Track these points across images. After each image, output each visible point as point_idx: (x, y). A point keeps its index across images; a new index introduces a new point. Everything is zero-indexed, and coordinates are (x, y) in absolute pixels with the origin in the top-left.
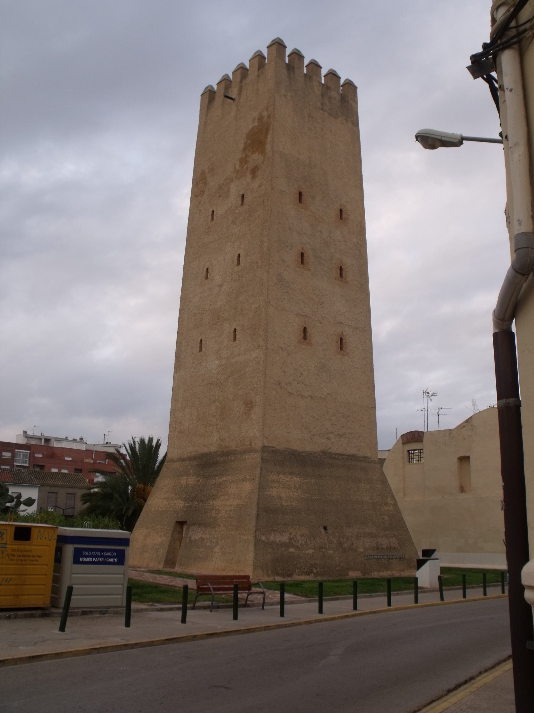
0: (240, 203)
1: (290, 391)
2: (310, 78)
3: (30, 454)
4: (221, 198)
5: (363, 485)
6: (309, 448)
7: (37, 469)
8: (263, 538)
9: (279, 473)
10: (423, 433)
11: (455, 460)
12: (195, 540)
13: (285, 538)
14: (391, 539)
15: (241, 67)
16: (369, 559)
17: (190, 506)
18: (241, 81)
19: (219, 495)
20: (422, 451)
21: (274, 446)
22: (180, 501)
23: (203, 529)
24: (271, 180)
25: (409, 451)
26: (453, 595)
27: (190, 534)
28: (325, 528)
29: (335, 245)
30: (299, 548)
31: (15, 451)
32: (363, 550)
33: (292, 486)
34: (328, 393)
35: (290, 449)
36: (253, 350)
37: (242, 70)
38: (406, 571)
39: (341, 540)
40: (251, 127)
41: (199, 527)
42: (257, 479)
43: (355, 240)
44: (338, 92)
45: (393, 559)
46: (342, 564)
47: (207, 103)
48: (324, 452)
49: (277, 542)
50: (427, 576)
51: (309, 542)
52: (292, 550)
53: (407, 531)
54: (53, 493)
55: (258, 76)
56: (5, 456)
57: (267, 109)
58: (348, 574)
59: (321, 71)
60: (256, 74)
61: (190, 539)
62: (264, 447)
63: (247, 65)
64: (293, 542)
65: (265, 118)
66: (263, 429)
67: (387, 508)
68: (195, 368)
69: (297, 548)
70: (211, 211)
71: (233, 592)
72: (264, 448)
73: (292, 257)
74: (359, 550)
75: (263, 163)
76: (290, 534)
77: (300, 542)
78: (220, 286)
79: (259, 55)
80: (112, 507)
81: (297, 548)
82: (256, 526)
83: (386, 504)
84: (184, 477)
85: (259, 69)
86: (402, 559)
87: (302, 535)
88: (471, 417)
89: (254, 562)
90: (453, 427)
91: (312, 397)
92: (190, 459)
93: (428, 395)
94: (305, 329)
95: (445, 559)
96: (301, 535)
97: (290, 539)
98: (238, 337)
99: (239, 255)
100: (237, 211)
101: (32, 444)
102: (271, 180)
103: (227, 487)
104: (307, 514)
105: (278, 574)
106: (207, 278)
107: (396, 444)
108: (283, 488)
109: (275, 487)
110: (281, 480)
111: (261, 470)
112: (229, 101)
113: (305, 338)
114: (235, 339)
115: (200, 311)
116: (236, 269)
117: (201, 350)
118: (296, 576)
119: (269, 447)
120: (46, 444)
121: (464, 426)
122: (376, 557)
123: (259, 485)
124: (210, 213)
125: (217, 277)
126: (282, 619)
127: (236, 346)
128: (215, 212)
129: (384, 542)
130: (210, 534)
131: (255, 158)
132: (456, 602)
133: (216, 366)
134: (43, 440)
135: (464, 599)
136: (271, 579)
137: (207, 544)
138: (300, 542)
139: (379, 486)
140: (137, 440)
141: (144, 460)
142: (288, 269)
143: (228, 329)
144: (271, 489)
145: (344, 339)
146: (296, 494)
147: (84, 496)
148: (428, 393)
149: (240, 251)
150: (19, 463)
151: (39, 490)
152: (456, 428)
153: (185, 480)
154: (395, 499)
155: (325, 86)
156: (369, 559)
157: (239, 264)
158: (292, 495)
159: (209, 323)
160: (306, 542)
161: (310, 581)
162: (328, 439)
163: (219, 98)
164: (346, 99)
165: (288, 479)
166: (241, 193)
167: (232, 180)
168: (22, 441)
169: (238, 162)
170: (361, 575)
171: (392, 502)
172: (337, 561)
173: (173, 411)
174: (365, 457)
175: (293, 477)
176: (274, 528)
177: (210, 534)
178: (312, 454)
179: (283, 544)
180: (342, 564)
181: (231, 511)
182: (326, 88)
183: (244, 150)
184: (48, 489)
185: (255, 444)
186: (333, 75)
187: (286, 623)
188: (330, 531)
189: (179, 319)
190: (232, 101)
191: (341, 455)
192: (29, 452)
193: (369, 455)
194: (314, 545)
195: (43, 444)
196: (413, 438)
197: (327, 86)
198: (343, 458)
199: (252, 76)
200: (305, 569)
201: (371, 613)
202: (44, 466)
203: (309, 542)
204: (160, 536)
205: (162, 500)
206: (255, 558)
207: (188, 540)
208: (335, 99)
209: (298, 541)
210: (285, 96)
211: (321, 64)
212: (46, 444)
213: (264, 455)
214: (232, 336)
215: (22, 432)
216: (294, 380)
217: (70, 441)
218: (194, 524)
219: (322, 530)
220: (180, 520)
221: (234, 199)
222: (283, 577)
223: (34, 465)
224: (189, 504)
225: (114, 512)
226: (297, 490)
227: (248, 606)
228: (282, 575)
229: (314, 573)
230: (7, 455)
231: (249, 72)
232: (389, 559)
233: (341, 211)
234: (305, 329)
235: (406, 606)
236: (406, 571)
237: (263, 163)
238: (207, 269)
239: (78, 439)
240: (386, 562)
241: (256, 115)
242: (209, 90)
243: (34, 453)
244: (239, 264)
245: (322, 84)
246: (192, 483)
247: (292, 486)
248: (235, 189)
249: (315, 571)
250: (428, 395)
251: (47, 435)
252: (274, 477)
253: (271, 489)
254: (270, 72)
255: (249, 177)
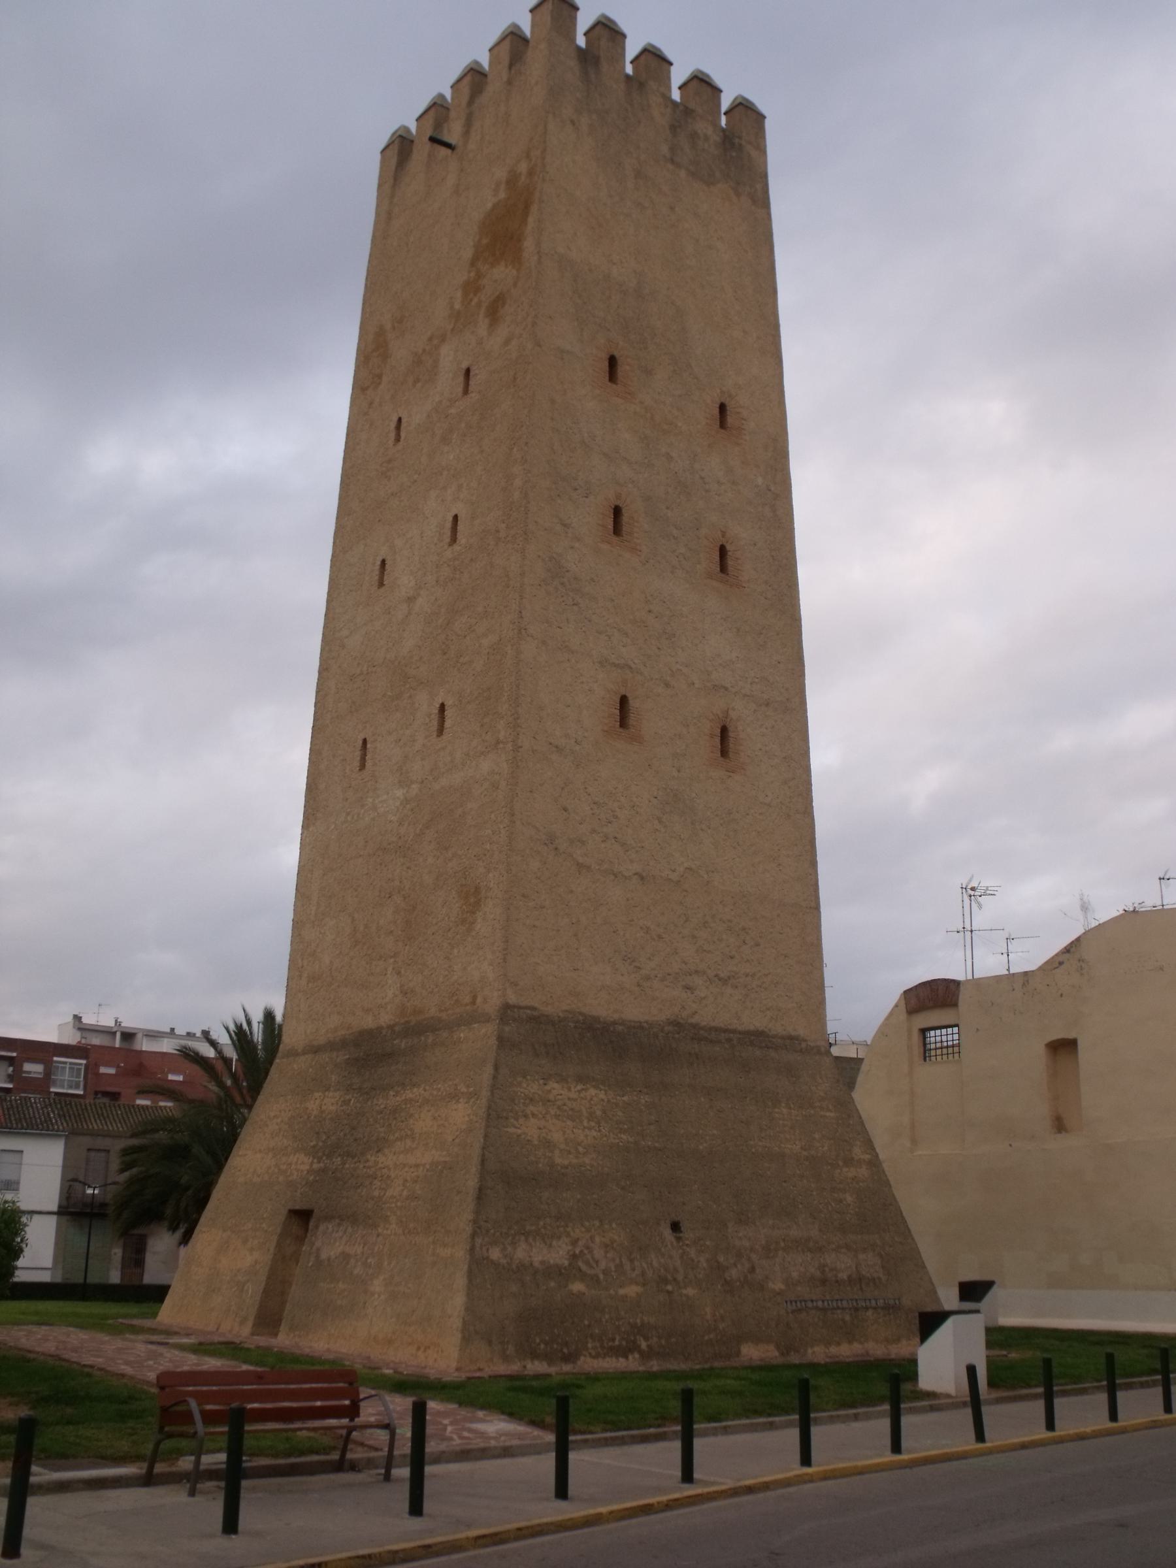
0: (460, 389)
1: (581, 860)
2: (642, 85)
3: (87, 1066)
4: (419, 385)
5: (785, 1111)
6: (634, 1012)
7: (106, 1100)
8: (495, 1254)
9: (546, 1079)
10: (957, 983)
11: (1040, 1049)
12: (329, 1260)
13: (558, 1254)
14: (861, 1256)
15: (472, 69)
16: (800, 1311)
17: (324, 1171)
18: (471, 102)
19: (391, 1137)
20: (956, 1030)
21: (536, 1005)
22: (302, 1157)
23: (350, 1230)
24: (534, 324)
25: (924, 1031)
26: (1015, 1421)
27: (318, 1244)
28: (675, 1227)
29: (707, 491)
30: (598, 1281)
31: (52, 1061)
32: (783, 1287)
33: (585, 1114)
34: (690, 869)
35: (581, 1013)
36: (482, 753)
37: (474, 77)
38: (904, 1342)
39: (721, 1259)
40: (489, 205)
41: (339, 1225)
42: (485, 1093)
43: (760, 481)
44: (715, 123)
45: (867, 1308)
46: (721, 1326)
47: (393, 168)
48: (677, 1024)
49: (536, 1264)
50: (943, 1361)
51: (627, 1266)
52: (577, 1287)
53: (906, 1233)
54: (99, 1150)
55: (509, 82)
56: (29, 1072)
57: (528, 156)
58: (738, 1354)
59: (669, 72)
60: (505, 78)
61: (318, 1257)
62: (507, 1007)
63: (485, 63)
64: (580, 1264)
65: (523, 178)
66: (505, 960)
67: (850, 1172)
68: (348, 814)
69: (594, 1281)
70: (395, 419)
71: (226, 1429)
72: (507, 1012)
73: (589, 518)
74: (771, 1285)
75: (515, 285)
76: (574, 1243)
77: (603, 1265)
78: (411, 600)
79: (512, 33)
80: (185, 1180)
81: (594, 1281)
82: (475, 1222)
83: (849, 1162)
84: (317, 1095)
85: (511, 66)
86: (891, 1309)
87: (607, 1247)
88: (1078, 939)
89: (464, 1322)
90: (1033, 967)
91: (642, 878)
92: (331, 1046)
93: (972, 893)
94: (624, 701)
95: (1014, 1310)
96: (606, 1246)
97: (574, 1257)
98: (448, 724)
99: (456, 518)
100: (453, 411)
101: (94, 1046)
102: (534, 324)
103: (411, 1116)
104: (623, 1188)
105: (535, 1355)
106: (381, 584)
107: (891, 1014)
108: (557, 1117)
109: (533, 1115)
110: (551, 1097)
111: (496, 1068)
112: (444, 151)
113: (623, 722)
114: (441, 730)
115: (365, 668)
116: (448, 554)
117: (363, 766)
118: (589, 1360)
119: (520, 1008)
120: (125, 1045)
121: (1061, 963)
122: (820, 1304)
123: (489, 1108)
124: (393, 425)
125: (403, 579)
126: (415, 1523)
127: (443, 748)
128: (404, 421)
129: (843, 1264)
130: (365, 1244)
131: (500, 274)
132: (1024, 1446)
133: (398, 804)
134: (118, 1035)
135: (1050, 1434)
136: (514, 1368)
137: (356, 1272)
138: (603, 1265)
139: (828, 1114)
140: (257, 1017)
141: (254, 1056)
142: (577, 545)
143: (425, 705)
144: (522, 1121)
145: (731, 729)
146: (594, 1133)
147: (126, 1152)
148: (973, 889)
149: (459, 508)
150: (63, 1087)
151: (66, 1144)
152: (1041, 968)
153: (318, 1102)
154: (874, 1149)
155: (681, 108)
156: (800, 1311)
157: (454, 539)
158: (582, 1137)
159: (384, 695)
160: (621, 1265)
161: (624, 1376)
162: (687, 988)
163: (422, 149)
164: (737, 141)
165: (573, 1095)
166: (464, 365)
167: (443, 339)
168: (70, 1038)
169: (459, 294)
170: (777, 1354)
171: (867, 1157)
172: (709, 1317)
173: (298, 925)
174: (791, 1038)
175: (586, 1090)
176: (528, 1228)
177: (365, 1244)
178: (642, 1028)
179: (550, 1271)
180: (721, 1326)
181: (416, 1181)
182: (682, 113)
183: (473, 263)
184: (86, 1141)
185: (485, 1000)
186: (701, 83)
187: (395, 1547)
188: (688, 1234)
189: (317, 692)
190: (449, 151)
191: (726, 1031)
192: (84, 1062)
193: (801, 1032)
194: (643, 1274)
195: (117, 1045)
196: (933, 998)
197: (687, 108)
198: (729, 1040)
199: (493, 87)
200: (613, 1340)
201: (735, 1492)
202: (119, 1094)
203: (627, 1266)
204: (252, 1250)
205: (264, 1158)
206: (469, 1309)
207: (312, 1259)
208: (706, 138)
209: (597, 1262)
210: (573, 122)
211: (670, 56)
212: (125, 1045)
213: (507, 1029)
214: (435, 723)
215: (70, 1019)
216: (594, 831)
217: (180, 1037)
218: (328, 1218)
219: (667, 1233)
220: (297, 1207)
221: (447, 382)
222: (551, 1363)
223: (96, 1093)
224: (322, 1165)
225: (190, 1192)
226: (599, 1123)
227: (354, 1467)
228: (548, 1358)
229: (641, 1352)
230: (34, 1069)
231: (490, 78)
232: (856, 1309)
233: (722, 408)
234: (624, 701)
235: (860, 1463)
236: (904, 1342)
237: (515, 285)
238: (383, 562)
239: (199, 1034)
240: (847, 1318)
241: (501, 174)
242: (400, 136)
243: (97, 1066)
244: (454, 539)
245: (674, 103)
246: (333, 1108)
247: (585, 1114)
248: (449, 359)
249: (644, 1345)
250: (972, 893)
251: (129, 1023)
252: (533, 1088)
253: (522, 1121)
254: (536, 64)
255: (482, 328)
